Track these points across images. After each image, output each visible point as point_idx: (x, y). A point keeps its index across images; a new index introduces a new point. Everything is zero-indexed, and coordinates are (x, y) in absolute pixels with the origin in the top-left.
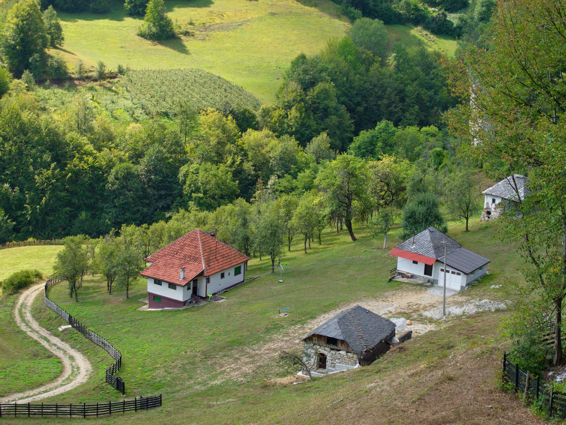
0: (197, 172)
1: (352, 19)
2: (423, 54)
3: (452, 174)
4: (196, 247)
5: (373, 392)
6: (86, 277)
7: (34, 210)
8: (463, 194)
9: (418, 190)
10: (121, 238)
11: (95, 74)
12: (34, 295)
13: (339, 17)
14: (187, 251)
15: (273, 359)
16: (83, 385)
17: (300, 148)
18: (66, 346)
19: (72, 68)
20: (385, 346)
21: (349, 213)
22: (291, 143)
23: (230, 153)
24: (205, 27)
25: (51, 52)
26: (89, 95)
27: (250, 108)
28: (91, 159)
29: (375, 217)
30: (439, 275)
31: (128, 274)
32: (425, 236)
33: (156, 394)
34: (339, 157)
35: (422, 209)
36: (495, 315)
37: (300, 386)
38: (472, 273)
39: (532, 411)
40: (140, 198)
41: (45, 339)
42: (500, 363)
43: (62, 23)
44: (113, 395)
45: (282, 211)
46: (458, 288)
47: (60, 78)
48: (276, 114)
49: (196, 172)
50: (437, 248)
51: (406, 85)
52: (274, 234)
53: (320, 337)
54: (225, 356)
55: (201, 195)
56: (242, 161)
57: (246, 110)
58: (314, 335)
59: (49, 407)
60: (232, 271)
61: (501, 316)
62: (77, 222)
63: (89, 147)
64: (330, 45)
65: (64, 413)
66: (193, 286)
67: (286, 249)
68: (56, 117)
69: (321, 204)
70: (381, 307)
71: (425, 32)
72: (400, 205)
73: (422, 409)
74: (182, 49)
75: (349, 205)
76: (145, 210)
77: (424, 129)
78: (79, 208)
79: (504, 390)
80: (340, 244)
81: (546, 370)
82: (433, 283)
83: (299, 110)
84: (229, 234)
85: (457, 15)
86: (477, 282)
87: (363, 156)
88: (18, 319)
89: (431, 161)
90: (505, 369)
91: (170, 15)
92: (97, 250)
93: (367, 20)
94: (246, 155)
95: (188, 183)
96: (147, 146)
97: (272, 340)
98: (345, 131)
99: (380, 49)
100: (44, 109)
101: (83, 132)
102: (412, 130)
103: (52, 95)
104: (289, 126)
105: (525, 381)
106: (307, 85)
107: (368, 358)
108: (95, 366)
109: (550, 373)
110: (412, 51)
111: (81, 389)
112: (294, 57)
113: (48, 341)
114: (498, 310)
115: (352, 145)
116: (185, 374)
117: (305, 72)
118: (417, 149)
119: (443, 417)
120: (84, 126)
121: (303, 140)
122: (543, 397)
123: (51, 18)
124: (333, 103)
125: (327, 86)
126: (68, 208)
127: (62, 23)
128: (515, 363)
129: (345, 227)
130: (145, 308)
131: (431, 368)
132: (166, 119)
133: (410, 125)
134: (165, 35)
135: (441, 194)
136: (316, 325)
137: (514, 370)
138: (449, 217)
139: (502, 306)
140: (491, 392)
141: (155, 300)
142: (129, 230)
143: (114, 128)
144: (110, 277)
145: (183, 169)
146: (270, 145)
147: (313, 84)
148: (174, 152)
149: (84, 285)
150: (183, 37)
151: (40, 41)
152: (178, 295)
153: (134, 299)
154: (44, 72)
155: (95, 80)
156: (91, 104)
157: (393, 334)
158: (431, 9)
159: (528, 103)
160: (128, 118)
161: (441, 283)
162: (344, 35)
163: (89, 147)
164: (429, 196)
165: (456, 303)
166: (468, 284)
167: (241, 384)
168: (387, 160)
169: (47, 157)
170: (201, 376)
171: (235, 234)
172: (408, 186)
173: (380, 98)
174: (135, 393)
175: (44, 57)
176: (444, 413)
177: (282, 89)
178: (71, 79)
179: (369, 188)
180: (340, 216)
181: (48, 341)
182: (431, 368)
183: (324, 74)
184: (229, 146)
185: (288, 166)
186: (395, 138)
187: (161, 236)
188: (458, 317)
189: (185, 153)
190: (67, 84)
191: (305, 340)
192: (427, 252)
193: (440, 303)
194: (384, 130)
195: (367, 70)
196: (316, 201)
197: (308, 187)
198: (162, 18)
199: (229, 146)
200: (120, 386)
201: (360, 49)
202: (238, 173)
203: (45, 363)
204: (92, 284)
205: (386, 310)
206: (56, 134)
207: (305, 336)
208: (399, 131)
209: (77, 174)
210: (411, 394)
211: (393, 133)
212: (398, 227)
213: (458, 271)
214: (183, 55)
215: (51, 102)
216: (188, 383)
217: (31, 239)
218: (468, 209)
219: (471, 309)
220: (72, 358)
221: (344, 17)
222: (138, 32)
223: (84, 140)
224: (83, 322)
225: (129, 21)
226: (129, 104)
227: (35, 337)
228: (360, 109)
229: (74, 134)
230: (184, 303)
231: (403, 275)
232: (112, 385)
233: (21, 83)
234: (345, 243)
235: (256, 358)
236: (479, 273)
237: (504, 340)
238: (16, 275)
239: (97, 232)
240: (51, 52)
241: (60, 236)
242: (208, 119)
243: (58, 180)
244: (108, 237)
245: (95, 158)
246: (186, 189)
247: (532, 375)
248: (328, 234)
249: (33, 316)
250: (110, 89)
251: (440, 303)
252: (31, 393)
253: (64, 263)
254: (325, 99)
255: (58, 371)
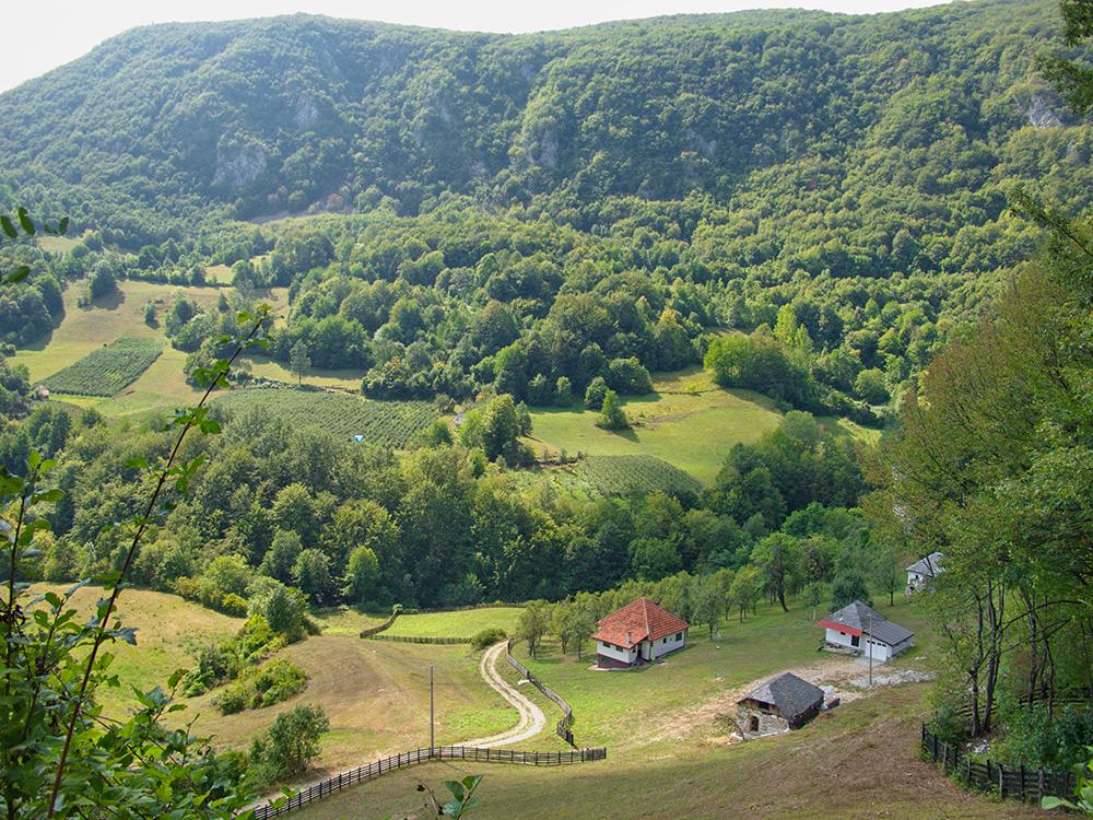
0: (644, 546)
1: (784, 412)
2: (850, 443)
3: (878, 552)
4: (642, 614)
5: (798, 755)
6: (543, 638)
7: (502, 576)
8: (889, 571)
9: (846, 566)
10: (575, 604)
11: (558, 459)
12: (498, 651)
13: (772, 410)
14: (634, 617)
15: (708, 720)
16: (536, 735)
17: (738, 526)
18: (523, 698)
19: (538, 454)
20: (813, 712)
21: (781, 586)
22: (729, 521)
23: (674, 529)
24: (654, 419)
25: (521, 439)
26: (552, 477)
27: (693, 490)
28: (552, 533)
29: (806, 591)
30: (865, 645)
31: (580, 637)
32: (852, 609)
33: (602, 747)
34: (772, 535)
35: (849, 584)
36: (920, 686)
37: (733, 747)
38: (897, 644)
39: (951, 780)
40: (594, 568)
41: (506, 691)
42: (920, 732)
43: (531, 415)
44: (564, 747)
45: (720, 584)
46: (885, 659)
47: (528, 462)
48: (717, 495)
49: (644, 547)
50: (863, 621)
51: (834, 470)
52: (712, 604)
53: (753, 701)
54: (665, 715)
55: (648, 567)
56: (685, 537)
57: (689, 492)
58: (747, 699)
59: (505, 753)
60: (674, 637)
61: (925, 687)
62: (538, 588)
63: (551, 522)
64: (765, 435)
65: (519, 759)
66: (638, 649)
67: (723, 618)
68: (523, 495)
69: (755, 578)
70: (809, 675)
71: (851, 423)
72: (829, 580)
73: (843, 773)
74: (634, 439)
75: (781, 579)
76: (598, 579)
77: (852, 509)
78: (540, 576)
79: (923, 759)
80: (773, 615)
81: (964, 740)
82: (860, 654)
83: (736, 492)
84: (671, 603)
85: (881, 408)
86: (902, 653)
87: (795, 534)
88: (483, 672)
89: (858, 539)
90: (924, 739)
91: (623, 408)
92: (554, 614)
93: (798, 412)
94: (688, 532)
95: (636, 556)
96: (601, 522)
97: (708, 702)
98: (778, 511)
99: (811, 438)
100: (514, 489)
101: (546, 509)
102: (840, 511)
103: (520, 476)
104: (727, 506)
105: (133, 409)
106: (745, 470)
107: (798, 723)
108: (548, 718)
109: (969, 745)
110: (839, 440)
111: (536, 739)
112: (732, 446)
113: (509, 694)
114: (922, 681)
115: (785, 524)
116: (629, 730)
117: (743, 458)
118: (845, 528)
119: (864, 783)
120: (547, 505)
121: (741, 519)
122: (960, 768)
123: (522, 411)
124: (768, 487)
125: (762, 470)
126: (531, 576)
127: (531, 415)
128: (933, 733)
129: (778, 599)
130: (595, 667)
131: (853, 735)
132: (619, 499)
133: (838, 506)
134: (618, 426)
135: (867, 571)
136: (747, 690)
137: (933, 740)
138: (876, 591)
139: (926, 677)
140: (911, 760)
141: (604, 661)
142: (582, 596)
143: (572, 506)
144: (564, 638)
145: (633, 543)
146: (711, 523)
147: (749, 469)
148: (624, 528)
149: (542, 644)
150: (634, 428)
151: (512, 430)
152: (624, 657)
153: (587, 660)
154: (515, 457)
155: (558, 464)
156: (554, 485)
157: (822, 700)
158: (855, 402)
159: (936, 488)
160: (586, 498)
161: (867, 654)
162: (778, 425)
163: (551, 522)
164: (856, 572)
165: (882, 673)
166: (893, 656)
167: (679, 742)
168: (816, 538)
169: (514, 530)
170: (642, 732)
171: (677, 603)
172: (836, 562)
173: (810, 482)
174: (584, 746)
175: (516, 444)
176: (865, 779)
177: (721, 473)
178: (538, 463)
179: (800, 563)
180: (773, 589)
181: (509, 694)
182: (853, 735)
183: (759, 460)
184: (673, 524)
185: (725, 540)
186: (824, 518)
187: (611, 603)
188: (885, 687)
189: (635, 529)
190: (534, 468)
191: (739, 703)
192: (854, 624)
193: (867, 672)
194: (816, 510)
195: (799, 457)
196: (751, 575)
197: (745, 561)
198: (616, 411)
199: (673, 524)
200: (569, 738)
201: (792, 438)
202: (681, 548)
203: (504, 713)
204: (549, 644)
205: (815, 678)
206: (523, 510)
207: (738, 700)
208: (828, 512)
209: (540, 545)
210: (833, 759)
211: (822, 514)
212: (826, 600)
213: (885, 643)
214: (634, 443)
215: (520, 483)
216: (630, 738)
217: (498, 602)
218: (892, 585)
219: (896, 679)
220: (528, 710)
221: (778, 410)
222: (596, 422)
223: (547, 516)
224: (540, 678)
225: (589, 414)
226: (586, 485)
227: (497, 689)
228: (792, 491)
229: (539, 511)
230: (630, 665)
231: (831, 645)
232: (563, 737)
233: (495, 466)
234: (778, 614)
235: (694, 718)
236: (905, 645)
237: (925, 710)
238: (484, 633)
239: (555, 598)
240: (521, 439)
241: (523, 600)
242: (656, 497)
243: (523, 551)
244: (564, 602)
245: (556, 532)
246: (635, 562)
247: (950, 746)
248: (762, 606)
249: (497, 670)
250: (570, 472)
251: (867, 672)
252: (491, 739)
253: (525, 624)
254: (761, 483)
255: (515, 720)
